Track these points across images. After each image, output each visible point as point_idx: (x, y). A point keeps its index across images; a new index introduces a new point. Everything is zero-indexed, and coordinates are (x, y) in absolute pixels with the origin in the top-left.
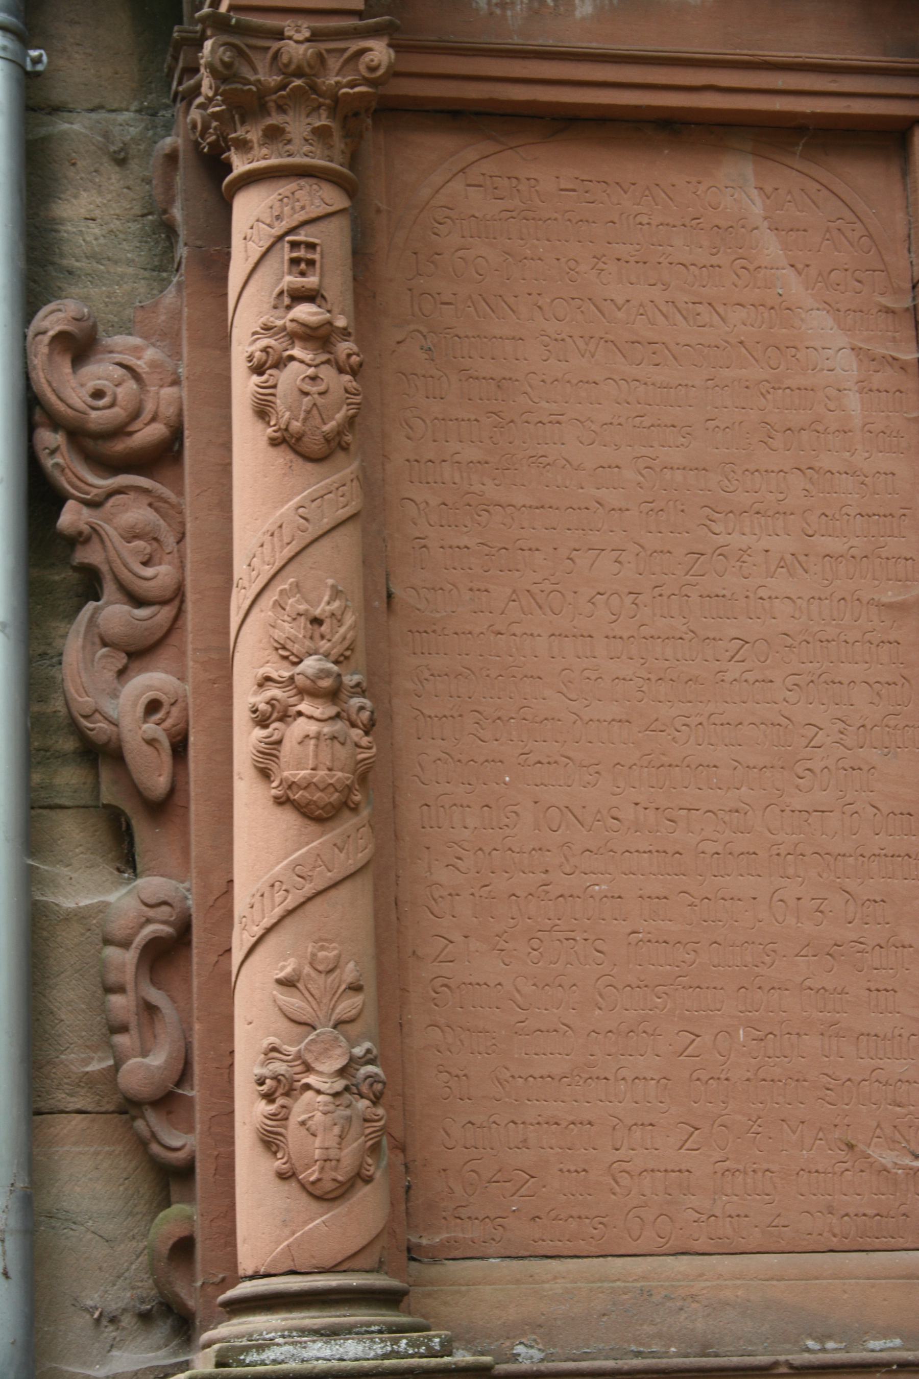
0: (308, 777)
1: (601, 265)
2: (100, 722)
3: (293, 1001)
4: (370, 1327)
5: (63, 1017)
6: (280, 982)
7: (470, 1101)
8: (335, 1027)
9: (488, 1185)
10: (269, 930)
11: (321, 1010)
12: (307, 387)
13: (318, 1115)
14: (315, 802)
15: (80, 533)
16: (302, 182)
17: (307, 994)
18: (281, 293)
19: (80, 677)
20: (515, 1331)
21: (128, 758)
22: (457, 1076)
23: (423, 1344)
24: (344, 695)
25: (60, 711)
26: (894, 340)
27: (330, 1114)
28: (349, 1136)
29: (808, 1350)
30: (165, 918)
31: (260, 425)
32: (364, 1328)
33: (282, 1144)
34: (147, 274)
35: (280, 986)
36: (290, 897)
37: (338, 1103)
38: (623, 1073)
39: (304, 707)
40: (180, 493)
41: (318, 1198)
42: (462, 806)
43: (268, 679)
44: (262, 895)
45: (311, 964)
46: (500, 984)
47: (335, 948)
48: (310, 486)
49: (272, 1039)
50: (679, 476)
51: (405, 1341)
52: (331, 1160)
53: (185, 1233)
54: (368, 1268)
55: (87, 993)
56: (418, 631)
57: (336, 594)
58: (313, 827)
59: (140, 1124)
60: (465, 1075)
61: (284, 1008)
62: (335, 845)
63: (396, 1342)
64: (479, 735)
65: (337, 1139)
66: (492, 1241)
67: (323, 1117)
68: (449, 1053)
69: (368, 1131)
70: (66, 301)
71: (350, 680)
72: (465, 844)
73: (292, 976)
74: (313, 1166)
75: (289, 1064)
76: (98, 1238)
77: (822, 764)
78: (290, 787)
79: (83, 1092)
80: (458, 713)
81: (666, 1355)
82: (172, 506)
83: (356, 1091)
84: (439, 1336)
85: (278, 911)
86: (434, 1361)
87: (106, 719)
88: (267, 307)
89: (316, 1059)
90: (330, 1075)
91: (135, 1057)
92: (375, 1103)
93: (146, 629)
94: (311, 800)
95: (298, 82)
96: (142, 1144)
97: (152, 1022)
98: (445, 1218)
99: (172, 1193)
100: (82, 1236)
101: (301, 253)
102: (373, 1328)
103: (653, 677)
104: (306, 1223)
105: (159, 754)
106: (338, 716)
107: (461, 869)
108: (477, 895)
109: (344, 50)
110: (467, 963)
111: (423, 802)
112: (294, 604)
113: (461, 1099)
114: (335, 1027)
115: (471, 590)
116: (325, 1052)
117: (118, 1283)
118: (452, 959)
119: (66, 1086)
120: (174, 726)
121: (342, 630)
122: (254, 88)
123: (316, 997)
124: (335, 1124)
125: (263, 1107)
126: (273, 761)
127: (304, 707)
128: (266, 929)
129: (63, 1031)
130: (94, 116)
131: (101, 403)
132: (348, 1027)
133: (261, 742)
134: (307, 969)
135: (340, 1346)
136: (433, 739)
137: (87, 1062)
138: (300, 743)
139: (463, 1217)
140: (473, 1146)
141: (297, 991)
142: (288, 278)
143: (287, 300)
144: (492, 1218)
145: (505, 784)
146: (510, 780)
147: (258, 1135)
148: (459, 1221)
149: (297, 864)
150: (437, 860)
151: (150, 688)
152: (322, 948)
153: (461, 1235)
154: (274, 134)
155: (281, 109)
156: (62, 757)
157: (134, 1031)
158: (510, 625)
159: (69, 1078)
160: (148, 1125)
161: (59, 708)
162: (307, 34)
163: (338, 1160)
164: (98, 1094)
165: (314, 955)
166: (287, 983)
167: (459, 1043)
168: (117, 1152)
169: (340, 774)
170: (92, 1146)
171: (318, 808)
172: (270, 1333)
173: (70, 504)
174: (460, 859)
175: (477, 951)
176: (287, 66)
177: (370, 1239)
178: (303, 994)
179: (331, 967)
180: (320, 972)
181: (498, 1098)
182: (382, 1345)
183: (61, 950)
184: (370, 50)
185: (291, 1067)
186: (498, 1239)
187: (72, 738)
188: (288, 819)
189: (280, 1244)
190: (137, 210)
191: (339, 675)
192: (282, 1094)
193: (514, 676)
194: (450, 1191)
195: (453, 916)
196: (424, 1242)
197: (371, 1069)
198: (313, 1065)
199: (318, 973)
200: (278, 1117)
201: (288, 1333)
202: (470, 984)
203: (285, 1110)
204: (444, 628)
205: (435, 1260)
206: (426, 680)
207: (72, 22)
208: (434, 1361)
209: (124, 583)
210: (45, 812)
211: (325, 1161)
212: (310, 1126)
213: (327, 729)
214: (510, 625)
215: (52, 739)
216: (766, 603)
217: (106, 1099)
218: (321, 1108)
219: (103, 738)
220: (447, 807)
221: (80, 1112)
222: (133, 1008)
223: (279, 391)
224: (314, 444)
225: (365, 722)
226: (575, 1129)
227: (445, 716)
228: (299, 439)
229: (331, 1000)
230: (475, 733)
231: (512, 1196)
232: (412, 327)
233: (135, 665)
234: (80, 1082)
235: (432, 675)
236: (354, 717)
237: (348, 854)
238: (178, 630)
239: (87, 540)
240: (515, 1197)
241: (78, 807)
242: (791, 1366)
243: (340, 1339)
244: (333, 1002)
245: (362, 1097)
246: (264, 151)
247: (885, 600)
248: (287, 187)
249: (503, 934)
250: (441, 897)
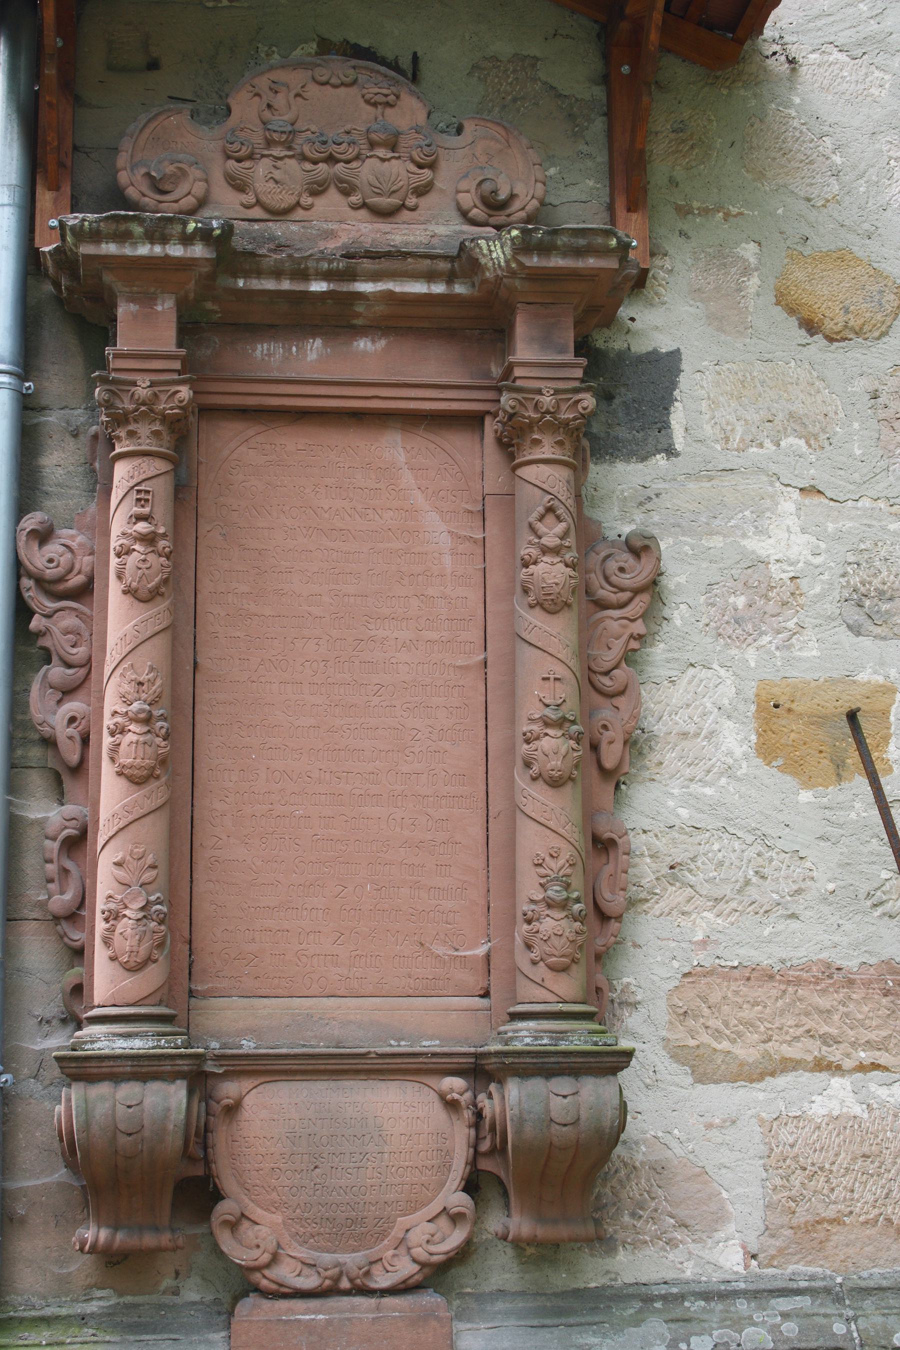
1: (317, 489)
3: (121, 873)
6: (116, 864)
8: (141, 886)
10: (111, 838)
12: (140, 566)
15: (40, 631)
16: (145, 459)
18: (131, 516)
20: (241, 1033)
21: (59, 745)
26: (471, 527)
29: (391, 1046)
31: (119, 583)
34: (86, 494)
38: (306, 906)
39: (132, 727)
40: (92, 610)
41: (128, 970)
43: (116, 712)
48: (141, 614)
49: (110, 892)
50: (352, 599)
57: (152, 669)
58: (135, 787)
59: (59, 927)
63: (159, 1041)
70: (37, 513)
71: (157, 713)
72: (230, 790)
77: (419, 750)
81: (318, 1046)
82: (88, 617)
85: (116, 829)
86: (174, 1051)
88: (125, 522)
90: (136, 910)
92: (160, 924)
95: (143, 408)
96: (62, 936)
97: (67, 877)
101: (142, 496)
103: (333, 705)
104: (122, 982)
106: (149, 731)
109: (168, 391)
112: (131, 675)
114: (141, 886)
116: (134, 899)
121: (154, 688)
122: (121, 411)
125: (117, 560)
127: (132, 727)
130: (62, 412)
131: (51, 565)
132: (148, 886)
134: (128, 858)
137: (38, 895)
142: (135, 509)
143: (134, 520)
149: (125, 805)
151: (71, 710)
152: (136, 847)
154: (132, 434)
155: (136, 421)
156: (33, 742)
162: (148, 384)
165: (132, 851)
166: (118, 864)
169: (148, 761)
173: (37, 615)
176: (138, 400)
184: (177, 392)
188: (122, 783)
190: (82, 461)
191: (150, 711)
196: (199, 988)
197: (159, 907)
201: (107, 1035)
205: (205, 997)
207: (53, 363)
208: (174, 1051)
210: (23, 770)
213: (142, 739)
216: (395, 666)
223: (127, 567)
224: (143, 593)
226: (280, 934)
228: (136, 591)
232: (216, 523)
233: (67, 698)
236: (157, 732)
239: (44, 634)
242: (377, 1054)
246: (127, 442)
247: (457, 664)
248: (137, 461)
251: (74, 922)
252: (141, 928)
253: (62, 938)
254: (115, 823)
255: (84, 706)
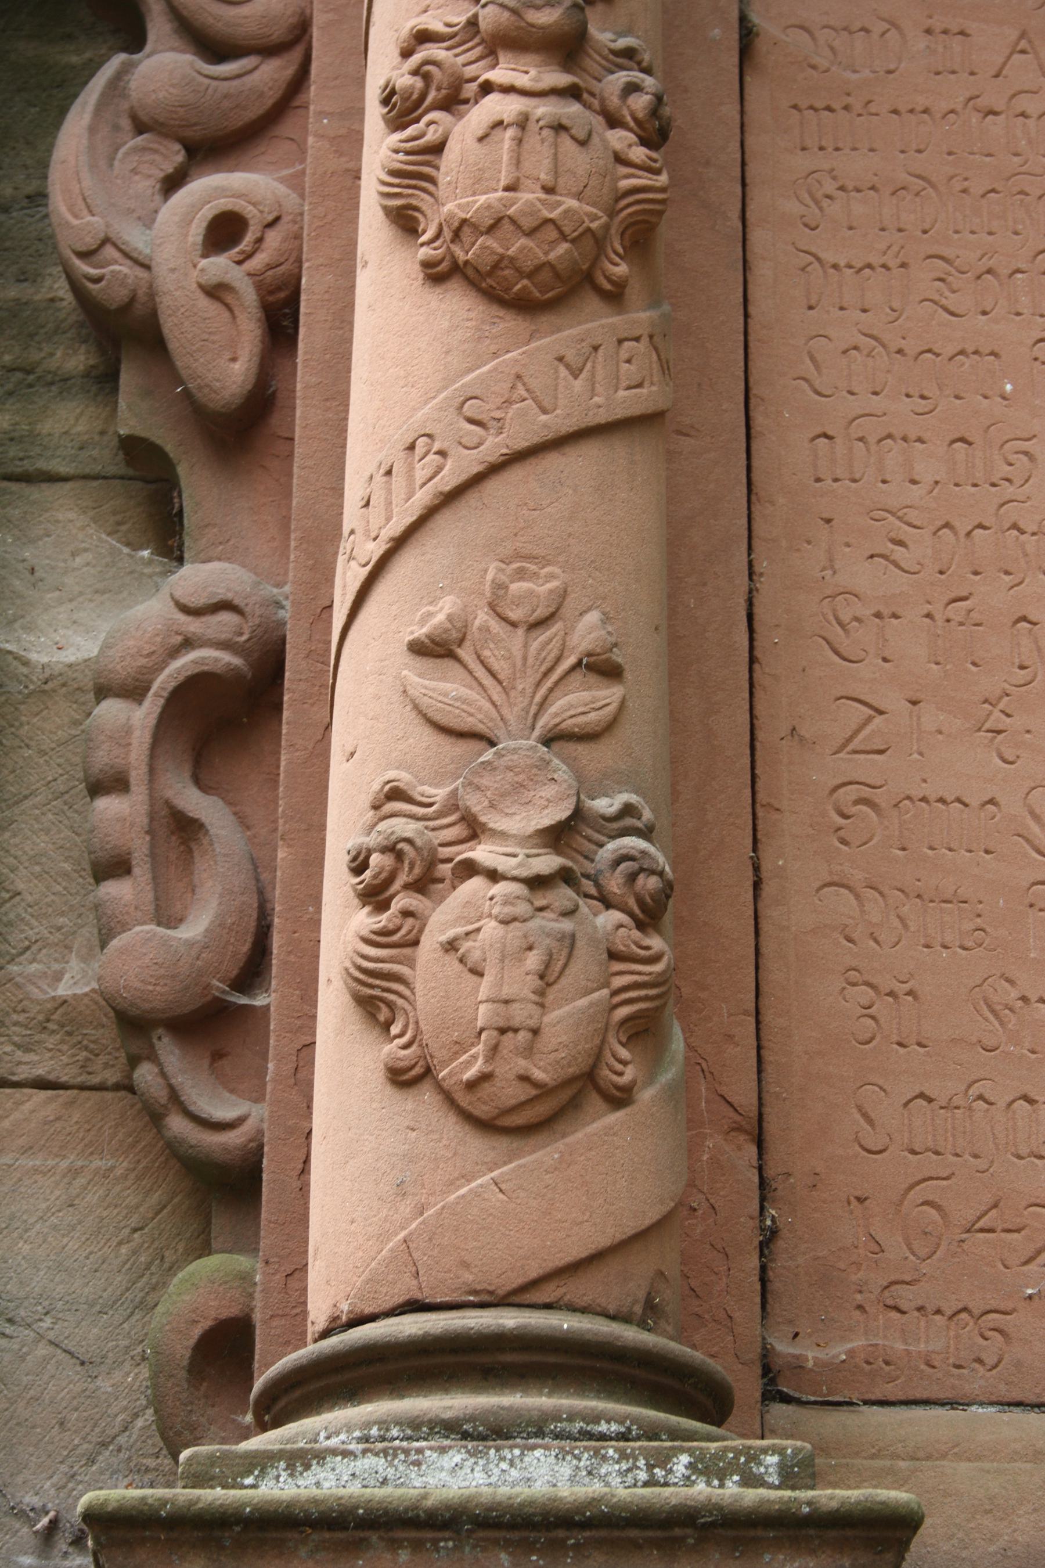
0: (496, 204)
2: (116, 262)
4: (598, 1423)
5: (20, 886)
6: (419, 649)
7: (922, 1050)
9: (965, 1236)
10: (399, 543)
11: (511, 705)
13: (490, 928)
14: (512, 260)
17: (480, 672)
19: (79, 181)
22: (891, 994)
23: (733, 1467)
24: (592, 63)
25: (62, 300)
27: (517, 924)
28: (564, 981)
30: (223, 636)
32: (579, 1425)
33: (400, 1002)
35: (418, 659)
36: (449, 464)
37: (540, 902)
42: (905, 439)
44: (389, 473)
45: (492, 606)
46: (992, 801)
47: (552, 577)
51: (685, 1459)
52: (516, 1031)
53: (233, 1311)
54: (612, 1309)
55: (78, 839)
56: (811, 108)
58: (510, 323)
60: (909, 993)
61: (424, 702)
62: (560, 359)
63: (663, 1460)
64: (944, 301)
65: (535, 982)
66: (976, 1365)
67: (501, 929)
68: (872, 943)
69: (618, 982)
72: (912, 516)
73: (446, 631)
74: (473, 1045)
75: (431, 824)
76: (61, 1355)
78: (457, 235)
79: (51, 1041)
80: (898, 261)
83: (593, 891)
84: (780, 1451)
85: (422, 498)
87: (126, 255)
89: (492, 806)
91: (144, 923)
93: (226, 96)
94: (502, 257)
98: (860, 1307)
99: (215, 1228)
100: (24, 1350)
102: (603, 1427)
104: (452, 1184)
105: (234, 317)
107: (903, 564)
108: (939, 617)
110: (916, 756)
111: (819, 430)
113: (900, 1044)
114: (548, 741)
115: (928, 31)
117: (100, 1458)
118: (882, 747)
119: (14, 1028)
120: (270, 267)
123: (501, 677)
124: (530, 948)
125: (364, 920)
126: (424, 190)
127: (498, 75)
128: (392, 539)
129: (18, 915)
133: (396, 151)
134: (483, 617)
135: (512, 1464)
136: (842, 309)
138: (481, 139)
139: (904, 1308)
140: (927, 1150)
141: (457, 665)
144: (976, 1312)
145: (1004, 398)
146: (1014, 390)
147: (345, 982)
148: (894, 1315)
150: (848, 545)
152: (521, 575)
153: (900, 1346)
157: (141, 870)
158: (1014, 96)
159: (24, 1011)
160: (163, 1074)
161: (61, 293)
163: (535, 1032)
164: (86, 1048)
165: (499, 587)
167: (896, 923)
168: (119, 1172)
170: (64, 1157)
171: (521, 273)
172: (337, 1433)
174: (900, 543)
175: (940, 732)
177: (620, 1237)
178: (470, 672)
179: (540, 613)
180: (514, 625)
181: (990, 1043)
182: (624, 1466)
183: (27, 753)
185: (433, 829)
186: (990, 1361)
187: (83, 348)
189: (389, 1240)
192: (407, 887)
193: (1022, 192)
194: (877, 1249)
195: (885, 660)
196: (811, 1355)
198: (483, 819)
199: (509, 628)
200: (395, 938)
202: (924, 799)
203: (410, 921)
204: (870, 102)
206: (828, 197)
209: (185, 13)
211: (502, 1031)
212: (468, 951)
214: (1014, 96)
215: (40, 349)
217: (102, 1059)
218: (495, 911)
219: (118, 296)
220: (872, 439)
221: (42, 1084)
222: (142, 820)
225: (640, 115)
227: (869, 266)
229: (538, 684)
230: (936, 297)
231: (1026, 1263)
234: (48, 1020)
235: (842, 188)
237: (592, 381)
238: (300, 111)
240: (1032, 1267)
241: (85, 477)
243: (511, 1448)
244: (542, 691)
245: (608, 905)
249: (1000, 698)
250: (857, 619)
251: (217, 1056)
252: (550, 923)
253: (155, 1117)
254: (421, 473)
255: (282, 189)
